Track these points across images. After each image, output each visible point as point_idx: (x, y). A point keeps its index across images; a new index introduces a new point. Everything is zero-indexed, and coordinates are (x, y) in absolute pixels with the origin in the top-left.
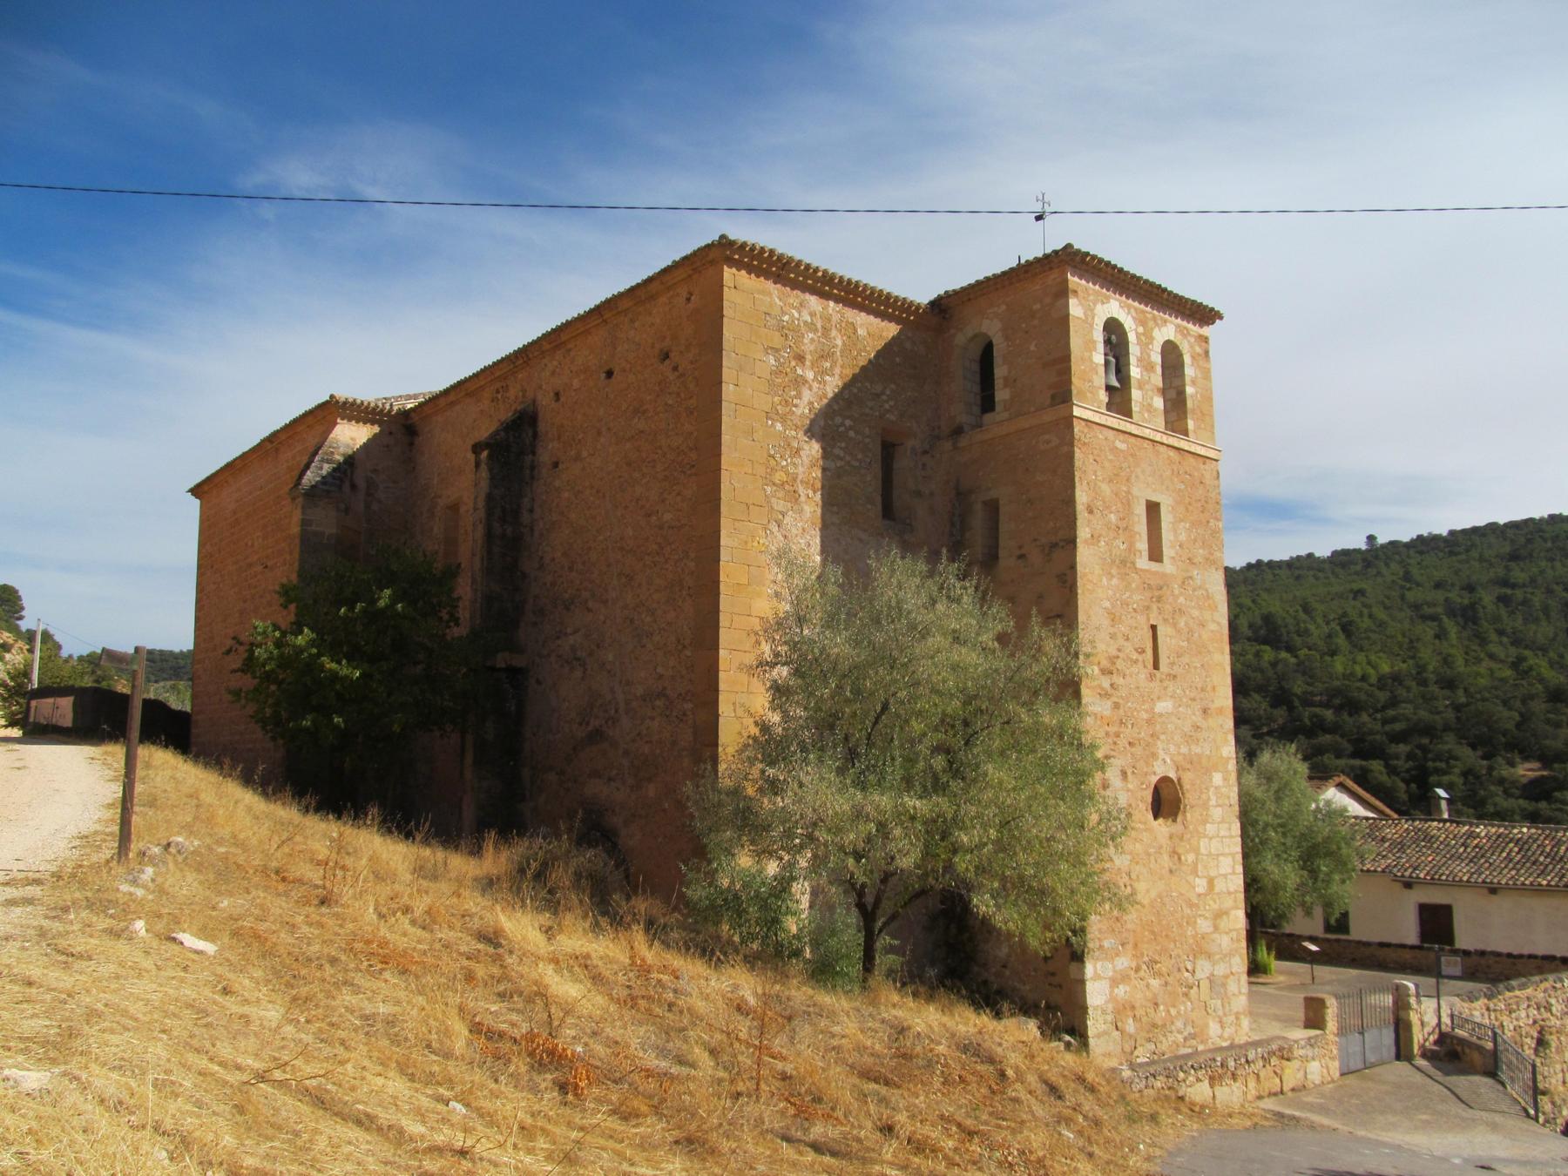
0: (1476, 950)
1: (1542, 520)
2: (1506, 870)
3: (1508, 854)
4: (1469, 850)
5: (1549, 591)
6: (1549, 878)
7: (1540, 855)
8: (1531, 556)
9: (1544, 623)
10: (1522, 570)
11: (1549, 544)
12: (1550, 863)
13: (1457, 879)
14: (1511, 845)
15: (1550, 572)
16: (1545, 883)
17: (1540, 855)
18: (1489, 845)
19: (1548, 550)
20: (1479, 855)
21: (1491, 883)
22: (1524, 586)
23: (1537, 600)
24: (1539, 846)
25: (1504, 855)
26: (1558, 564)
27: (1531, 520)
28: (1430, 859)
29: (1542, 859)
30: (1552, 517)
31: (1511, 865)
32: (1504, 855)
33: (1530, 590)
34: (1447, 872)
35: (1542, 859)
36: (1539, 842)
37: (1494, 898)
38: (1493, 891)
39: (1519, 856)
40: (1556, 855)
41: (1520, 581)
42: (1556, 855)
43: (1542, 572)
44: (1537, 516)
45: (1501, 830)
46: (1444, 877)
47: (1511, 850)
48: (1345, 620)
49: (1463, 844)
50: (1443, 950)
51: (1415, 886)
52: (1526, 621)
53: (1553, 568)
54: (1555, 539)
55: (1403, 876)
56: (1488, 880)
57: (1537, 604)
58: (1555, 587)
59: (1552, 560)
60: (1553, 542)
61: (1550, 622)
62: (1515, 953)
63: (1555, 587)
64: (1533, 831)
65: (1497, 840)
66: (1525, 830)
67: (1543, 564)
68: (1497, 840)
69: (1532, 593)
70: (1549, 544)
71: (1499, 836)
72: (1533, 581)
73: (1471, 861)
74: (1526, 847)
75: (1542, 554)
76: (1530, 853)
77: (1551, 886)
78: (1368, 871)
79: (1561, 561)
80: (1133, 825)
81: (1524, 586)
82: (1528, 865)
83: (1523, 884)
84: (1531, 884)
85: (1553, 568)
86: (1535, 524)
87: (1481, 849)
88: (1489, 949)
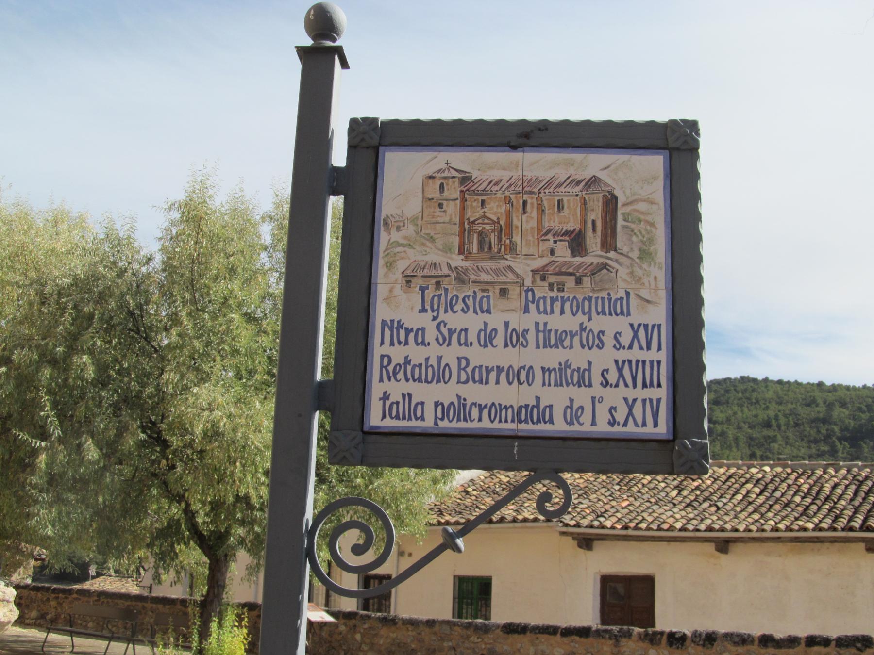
0: (696, 634)
1: (735, 379)
2: (745, 514)
3: (745, 497)
4: (685, 493)
5: (739, 428)
6: (816, 520)
7: (795, 494)
8: (728, 402)
9: (734, 449)
10: (721, 412)
11: (740, 395)
12: (812, 503)
13: (665, 526)
14: (749, 486)
15: (740, 414)
16: (810, 526)
17: (795, 494)
18: (716, 486)
19: (739, 399)
20: (701, 499)
21: (722, 530)
22: (722, 423)
23: (731, 432)
24: (789, 486)
25: (739, 497)
26: (746, 409)
27: (729, 379)
28: (625, 504)
29: (797, 499)
30: (742, 378)
31: (751, 509)
32: (739, 497)
33: (725, 426)
34: (650, 519)
35: (797, 499)
36: (790, 482)
37: (724, 559)
38: (724, 546)
39: (762, 498)
40: (818, 493)
41: (720, 420)
42: (818, 493)
43: (735, 413)
44: (732, 376)
45: (733, 470)
46: (643, 525)
47: (748, 492)
48: (642, 637)
49: (676, 487)
50: (628, 635)
51: (596, 544)
52: (722, 447)
53: (742, 411)
54: (744, 391)
55: (577, 525)
56: (716, 527)
57: (730, 436)
58: (743, 425)
59: (741, 406)
60: (743, 393)
61: (738, 450)
62: (779, 635)
63: (743, 425)
64: (779, 469)
65: (727, 480)
66: (767, 469)
67: (735, 408)
68: (727, 480)
69: (728, 428)
70: (740, 395)
71: (730, 477)
72: (728, 420)
73: (688, 505)
74: (771, 487)
75: (736, 402)
76: (778, 494)
77: (821, 530)
78: (525, 520)
79: (748, 407)
80: (127, 449)
81: (722, 423)
82: (777, 507)
83: (775, 529)
84: (788, 529)
85: (742, 411)
86: (730, 382)
87: (702, 491)
88: (722, 630)
